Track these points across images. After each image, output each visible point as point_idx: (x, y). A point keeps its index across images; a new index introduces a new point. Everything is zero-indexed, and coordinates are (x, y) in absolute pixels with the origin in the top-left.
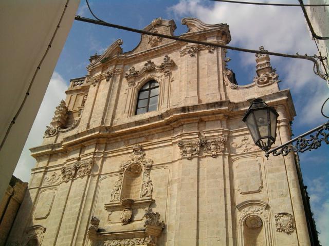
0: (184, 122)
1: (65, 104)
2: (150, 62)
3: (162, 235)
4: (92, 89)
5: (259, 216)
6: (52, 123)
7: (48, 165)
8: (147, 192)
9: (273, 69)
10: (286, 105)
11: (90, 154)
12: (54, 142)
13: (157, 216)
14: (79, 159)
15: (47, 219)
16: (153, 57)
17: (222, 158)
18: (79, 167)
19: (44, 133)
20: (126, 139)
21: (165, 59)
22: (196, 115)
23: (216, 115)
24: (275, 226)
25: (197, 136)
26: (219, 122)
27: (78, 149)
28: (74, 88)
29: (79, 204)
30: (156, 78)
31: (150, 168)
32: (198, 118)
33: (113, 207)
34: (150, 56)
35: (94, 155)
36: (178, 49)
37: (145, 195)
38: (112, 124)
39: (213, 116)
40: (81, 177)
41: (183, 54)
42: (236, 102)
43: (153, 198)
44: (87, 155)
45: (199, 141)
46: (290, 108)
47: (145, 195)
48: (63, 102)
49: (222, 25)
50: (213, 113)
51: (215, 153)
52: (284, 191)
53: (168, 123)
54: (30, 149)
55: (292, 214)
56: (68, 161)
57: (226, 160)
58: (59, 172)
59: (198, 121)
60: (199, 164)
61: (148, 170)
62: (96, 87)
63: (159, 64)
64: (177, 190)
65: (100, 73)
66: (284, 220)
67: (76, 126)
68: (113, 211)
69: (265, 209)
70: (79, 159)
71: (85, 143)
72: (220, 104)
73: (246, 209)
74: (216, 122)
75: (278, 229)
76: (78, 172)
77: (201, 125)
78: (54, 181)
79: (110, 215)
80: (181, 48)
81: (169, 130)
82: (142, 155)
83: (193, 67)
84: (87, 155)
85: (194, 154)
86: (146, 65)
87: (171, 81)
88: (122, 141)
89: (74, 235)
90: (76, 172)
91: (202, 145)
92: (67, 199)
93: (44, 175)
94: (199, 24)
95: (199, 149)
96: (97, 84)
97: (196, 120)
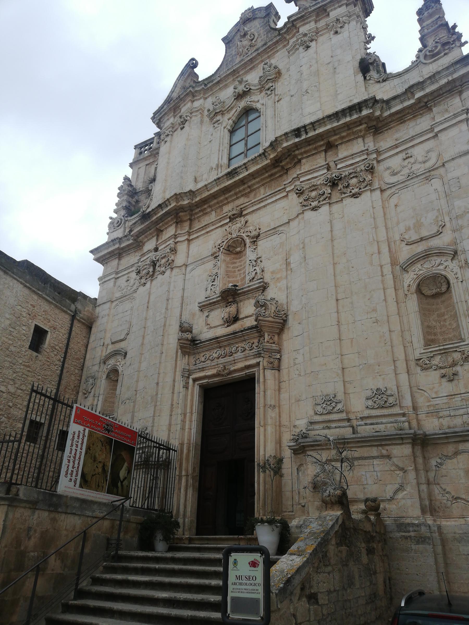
5: (443, 273)
6: (116, 211)
7: (118, 269)
8: (256, 273)
11: (169, 238)
14: (156, 250)
15: (127, 341)
17: (362, 141)
18: (158, 261)
20: (218, 206)
22: (320, 137)
25: (325, 171)
27: (153, 237)
28: (142, 157)
30: (255, 105)
31: (256, 239)
33: (210, 304)
36: (285, 46)
40: (161, 273)
43: (266, 281)
44: (165, 241)
47: (253, 278)
48: (126, 178)
50: (348, 126)
53: (276, 162)
54: (92, 252)
56: (143, 255)
58: (134, 275)
59: (324, 148)
61: (254, 242)
68: (212, 310)
69: (452, 260)
73: (418, 266)
74: (355, 141)
76: (157, 267)
79: (207, 316)
80: (288, 43)
82: (243, 222)
83: (311, 66)
84: (165, 241)
85: (323, 201)
87: (278, 101)
88: (212, 210)
90: (154, 269)
93: (115, 283)
95: (329, 191)
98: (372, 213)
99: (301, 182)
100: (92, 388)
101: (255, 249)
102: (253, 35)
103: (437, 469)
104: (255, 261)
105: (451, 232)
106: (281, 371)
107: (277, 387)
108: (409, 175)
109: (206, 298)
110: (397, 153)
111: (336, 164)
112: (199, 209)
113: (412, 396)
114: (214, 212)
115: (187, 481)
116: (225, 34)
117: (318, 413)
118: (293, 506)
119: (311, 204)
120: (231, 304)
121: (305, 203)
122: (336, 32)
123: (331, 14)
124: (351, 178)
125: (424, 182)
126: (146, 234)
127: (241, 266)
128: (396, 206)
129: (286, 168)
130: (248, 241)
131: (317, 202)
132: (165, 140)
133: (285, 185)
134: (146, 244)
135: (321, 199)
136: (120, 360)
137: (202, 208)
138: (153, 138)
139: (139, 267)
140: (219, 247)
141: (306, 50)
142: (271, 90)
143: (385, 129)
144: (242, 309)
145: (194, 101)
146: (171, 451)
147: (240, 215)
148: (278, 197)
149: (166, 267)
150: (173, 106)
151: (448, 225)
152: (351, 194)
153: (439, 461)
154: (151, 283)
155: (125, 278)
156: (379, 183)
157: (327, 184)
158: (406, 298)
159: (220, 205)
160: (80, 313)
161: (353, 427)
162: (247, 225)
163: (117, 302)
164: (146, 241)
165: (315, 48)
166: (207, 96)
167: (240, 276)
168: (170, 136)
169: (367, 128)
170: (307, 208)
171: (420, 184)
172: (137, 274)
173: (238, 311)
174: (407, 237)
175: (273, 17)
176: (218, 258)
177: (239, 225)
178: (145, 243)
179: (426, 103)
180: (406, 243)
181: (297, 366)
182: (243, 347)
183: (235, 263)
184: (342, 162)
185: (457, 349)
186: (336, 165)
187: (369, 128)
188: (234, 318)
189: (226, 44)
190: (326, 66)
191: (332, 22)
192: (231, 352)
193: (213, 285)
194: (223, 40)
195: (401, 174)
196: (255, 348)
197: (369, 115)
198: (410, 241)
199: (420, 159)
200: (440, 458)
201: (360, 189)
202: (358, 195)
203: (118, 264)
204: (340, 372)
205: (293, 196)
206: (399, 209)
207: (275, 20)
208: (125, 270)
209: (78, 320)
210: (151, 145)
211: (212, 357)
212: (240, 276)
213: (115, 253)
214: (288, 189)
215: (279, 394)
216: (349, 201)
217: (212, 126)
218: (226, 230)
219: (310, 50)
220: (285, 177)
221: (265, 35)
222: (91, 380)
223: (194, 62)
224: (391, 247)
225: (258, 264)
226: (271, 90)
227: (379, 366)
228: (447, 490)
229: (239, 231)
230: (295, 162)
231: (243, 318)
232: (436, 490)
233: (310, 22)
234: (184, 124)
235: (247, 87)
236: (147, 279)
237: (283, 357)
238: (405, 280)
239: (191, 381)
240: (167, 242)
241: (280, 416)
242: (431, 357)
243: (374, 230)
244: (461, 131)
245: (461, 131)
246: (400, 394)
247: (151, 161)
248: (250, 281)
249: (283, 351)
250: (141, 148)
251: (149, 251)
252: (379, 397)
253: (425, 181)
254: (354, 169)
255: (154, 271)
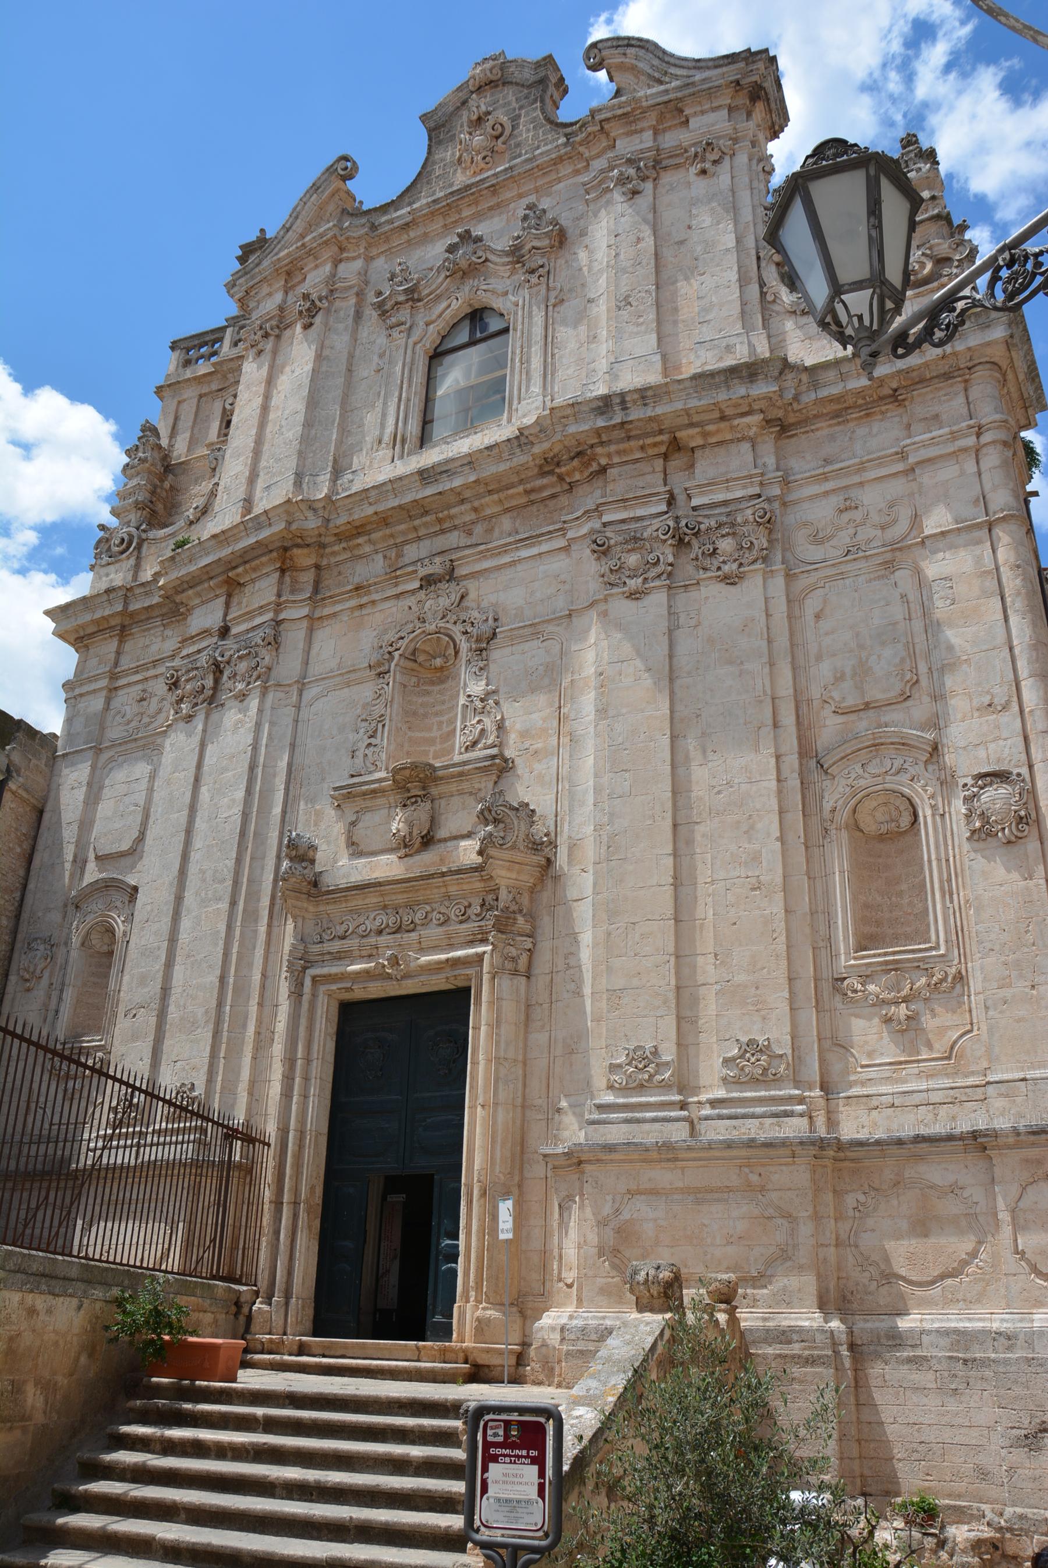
0: (609, 456)
1: (157, 435)
2: (466, 237)
3: (549, 883)
4: (252, 371)
9: (957, 221)
10: (1004, 364)
12: (130, 578)
13: (522, 814)
14: (224, 632)
16: (479, 217)
19: (92, 552)
21: (525, 218)
23: (736, 422)
24: (963, 822)
26: (746, 446)
27: (217, 596)
28: (188, 374)
29: (240, 794)
32: (665, 438)
34: (466, 213)
35: (277, 612)
36: (577, 172)
37: (475, 743)
38: (333, 490)
39: (723, 425)
40: (236, 697)
41: (598, 190)
42: (809, 362)
43: (508, 754)
44: (250, 615)
45: (671, 523)
46: (1021, 377)
47: (475, 743)
49: (748, 56)
51: (735, 566)
52: (996, 690)
54: (47, 613)
55: (1024, 771)
56: (185, 641)
57: (778, 583)
58: (160, 687)
60: (671, 613)
62: (266, 358)
63: (503, 244)
64: (592, 717)
65: (278, 297)
66: (995, 796)
67: (204, 511)
70: (224, 632)
71: (240, 570)
72: (749, 371)
75: (973, 832)
76: (225, 678)
77: (677, 462)
78: (146, 720)
79: (353, 824)
81: (553, 496)
82: (455, 597)
83: (639, 240)
84: (250, 615)
85: (654, 579)
86: (452, 249)
87: (554, 306)
88: (376, 552)
89: (233, 903)
90: (217, 681)
91: (681, 540)
92: (197, 780)
93: (108, 701)
94: (656, 62)
95: (671, 559)
96: (269, 345)
97: (655, 445)
98: (765, 629)
99: (605, 525)
100: (46, 967)
101: (481, 669)
102: (501, 125)
103: (857, 1214)
104: (482, 700)
105: (928, 699)
106: (533, 979)
107: (523, 1017)
108: (849, 551)
109: (352, 776)
110: (826, 493)
111: (688, 495)
112: (344, 545)
113: (822, 1061)
114: (380, 555)
115: (295, 1216)
116: (430, 107)
117: (617, 1085)
118: (544, 1283)
119: (625, 583)
120: (416, 802)
121: (613, 578)
122: (704, 172)
123: (693, 123)
124: (723, 536)
125: (879, 573)
126: (199, 588)
127: (443, 702)
128: (818, 617)
129: (568, 480)
130: (464, 646)
131: (640, 580)
132: (260, 347)
133: (564, 522)
134: (197, 612)
135: (651, 574)
136: (118, 904)
137: (351, 543)
138: (223, 329)
139: (177, 671)
140: (390, 649)
141: (631, 199)
142: (540, 276)
143: (802, 430)
144: (443, 817)
145: (341, 261)
146: (257, 1144)
147: (450, 575)
148: (545, 547)
149: (249, 683)
150: (286, 265)
151: (924, 682)
152: (719, 573)
153: (862, 1198)
154: (207, 717)
155: (135, 691)
156: (783, 557)
157: (665, 541)
158: (824, 838)
159: (398, 541)
160: (19, 775)
161: (692, 1123)
162: (464, 604)
163: (111, 753)
164: (198, 606)
165: (651, 199)
166: (374, 252)
167: (440, 729)
168: (272, 338)
169: (764, 423)
170: (615, 590)
171: (872, 576)
172: (170, 689)
173: (433, 821)
174: (836, 695)
175: (552, 89)
176: (387, 676)
177: (444, 602)
178: (193, 608)
179: (896, 390)
180: (833, 709)
181: (572, 971)
182: (443, 914)
183: (428, 693)
184: (702, 493)
185: (921, 964)
186: (689, 497)
187: (767, 422)
188: (422, 837)
189: (430, 131)
190: (676, 247)
191: (694, 145)
192: (412, 922)
193: (370, 745)
194: (424, 118)
195: (831, 543)
196: (473, 917)
197: (771, 395)
198: (842, 705)
199: (875, 518)
200: (865, 1193)
201: (741, 565)
202: (736, 580)
203: (118, 653)
204: (672, 996)
205: (584, 552)
206: (825, 625)
207: (556, 96)
208: (137, 672)
209: (13, 793)
210: (217, 346)
211: (363, 928)
212: (440, 729)
213: (113, 623)
214: (570, 534)
215: (526, 1032)
216: (713, 592)
217: (385, 332)
218: (410, 608)
219: (639, 200)
220: (564, 500)
221: (528, 130)
222: (41, 947)
223: (349, 164)
224: (800, 712)
225: (488, 707)
226: (540, 276)
227: (757, 988)
228: (872, 1259)
229: (444, 617)
230: (591, 470)
231: (445, 840)
232: (851, 1258)
233: (642, 131)
234: (313, 317)
235: (480, 253)
236: (196, 704)
237: (539, 946)
238: (826, 797)
239: (308, 982)
240: (254, 617)
241: (525, 1085)
242: (867, 976)
243: (767, 670)
244: (962, 473)
245: (962, 473)
246: (796, 1053)
247: (214, 387)
248: (467, 748)
249: (539, 931)
250: (188, 350)
251: (206, 633)
252: (753, 1060)
253: (883, 572)
254: (728, 514)
255: (216, 688)
